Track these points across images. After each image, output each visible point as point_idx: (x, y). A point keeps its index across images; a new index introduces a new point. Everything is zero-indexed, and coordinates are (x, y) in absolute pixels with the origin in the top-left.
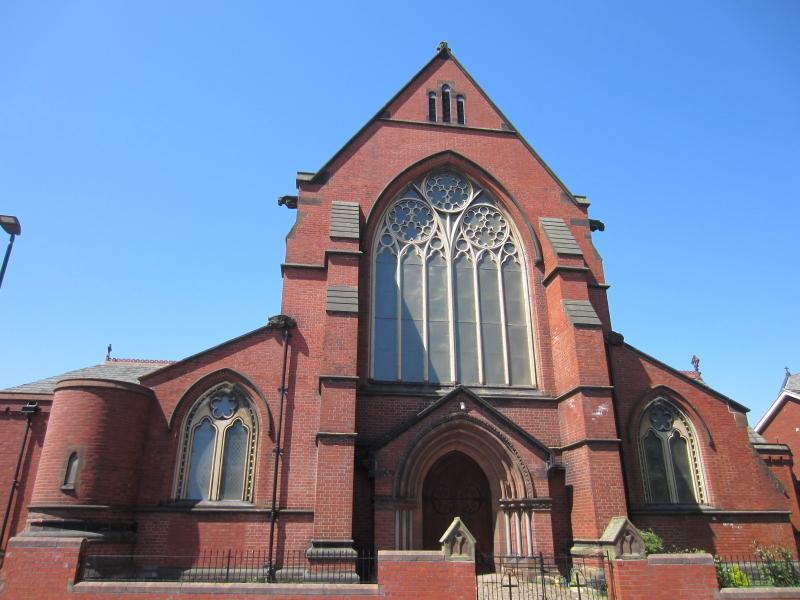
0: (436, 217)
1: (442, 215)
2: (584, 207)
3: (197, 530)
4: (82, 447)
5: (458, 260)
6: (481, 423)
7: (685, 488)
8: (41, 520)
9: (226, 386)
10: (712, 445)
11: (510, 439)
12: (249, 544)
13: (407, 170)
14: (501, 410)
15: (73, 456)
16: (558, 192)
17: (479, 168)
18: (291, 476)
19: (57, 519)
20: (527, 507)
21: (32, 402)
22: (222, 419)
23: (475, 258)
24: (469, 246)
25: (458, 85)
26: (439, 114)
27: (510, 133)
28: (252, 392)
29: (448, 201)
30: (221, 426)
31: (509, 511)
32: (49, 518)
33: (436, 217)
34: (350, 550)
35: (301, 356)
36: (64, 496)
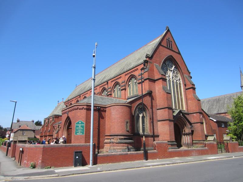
0: (169, 71)
1: (170, 70)
2: (190, 73)
3: (141, 139)
4: (128, 121)
5: (173, 82)
6: (182, 118)
7: (138, 131)
8: (123, 138)
9: (140, 106)
10: (206, 123)
11: (187, 123)
12: (150, 142)
13: (177, 62)
14: (185, 115)
15: (127, 123)
16: (186, 69)
17: (176, 61)
18: (154, 127)
19: (127, 137)
20: (187, 134)
21: (99, 107)
22: (141, 114)
23: (175, 81)
24: (174, 79)
25: (171, 39)
26: (168, 46)
27: (179, 53)
28: (147, 109)
29: (170, 67)
30: (141, 115)
31: (184, 135)
32: (125, 137)
33: (169, 71)
34: (175, 143)
35: (153, 100)
36: (127, 132)
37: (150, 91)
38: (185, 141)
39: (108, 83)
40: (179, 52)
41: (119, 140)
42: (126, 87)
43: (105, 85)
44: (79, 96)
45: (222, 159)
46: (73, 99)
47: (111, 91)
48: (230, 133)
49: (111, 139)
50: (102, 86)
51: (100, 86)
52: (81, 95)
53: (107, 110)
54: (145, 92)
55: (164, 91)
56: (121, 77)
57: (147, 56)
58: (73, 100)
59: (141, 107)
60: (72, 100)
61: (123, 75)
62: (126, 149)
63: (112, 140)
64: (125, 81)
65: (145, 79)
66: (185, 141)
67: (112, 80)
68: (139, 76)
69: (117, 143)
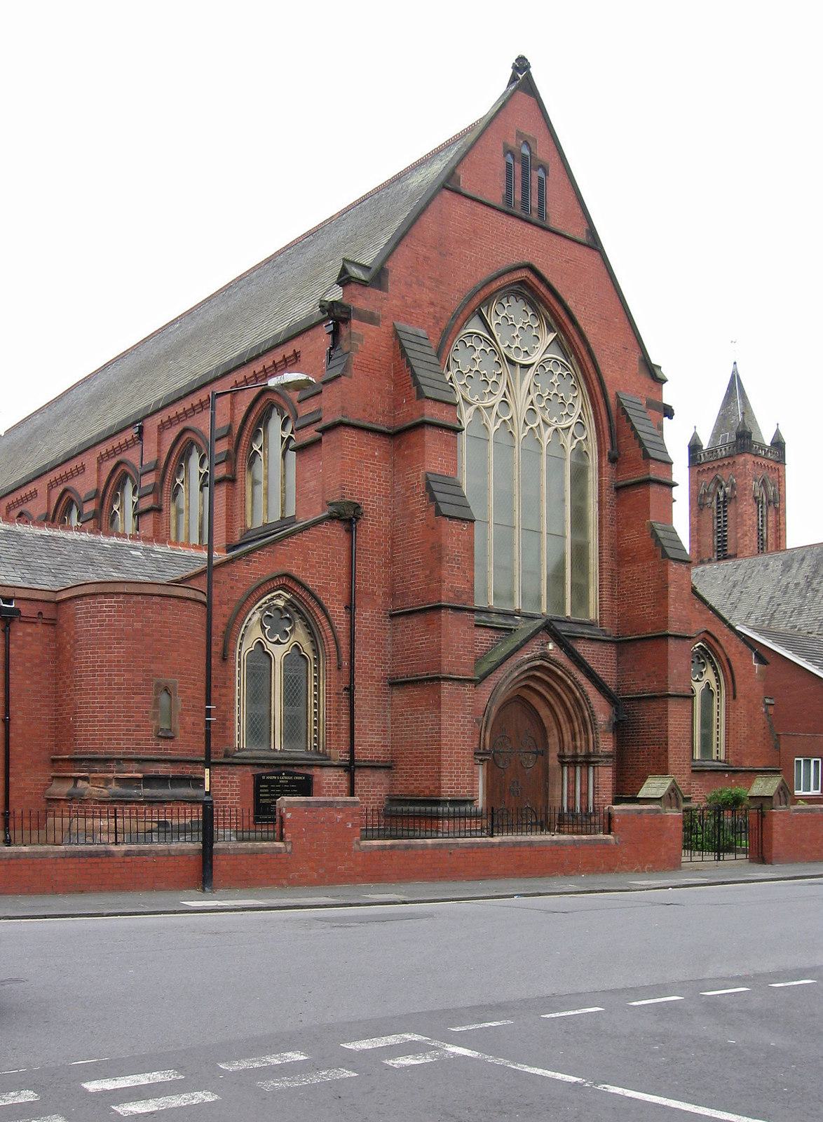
6: (558, 665)
9: (279, 596)
24: (539, 420)
37: (350, 503)
38: (572, 797)
39: (141, 432)
40: (592, 231)
41: (115, 788)
42: (239, 467)
43: (127, 446)
44: (133, 432)
45: (143, 1079)
46: (31, 488)
47: (95, 512)
48: (761, 808)
49: (76, 779)
50: (109, 455)
51: (103, 449)
52: (152, 425)
53: (319, 508)
54: (324, 511)
55: (433, 509)
56: (296, 355)
57: (344, 271)
58: (34, 494)
59: (281, 603)
60: (73, 465)
61: (90, 460)
62: (151, 831)
63: (81, 784)
64: (230, 427)
65: (327, 421)
66: (572, 797)
67: (103, 449)
68: (299, 402)
69: (101, 802)
